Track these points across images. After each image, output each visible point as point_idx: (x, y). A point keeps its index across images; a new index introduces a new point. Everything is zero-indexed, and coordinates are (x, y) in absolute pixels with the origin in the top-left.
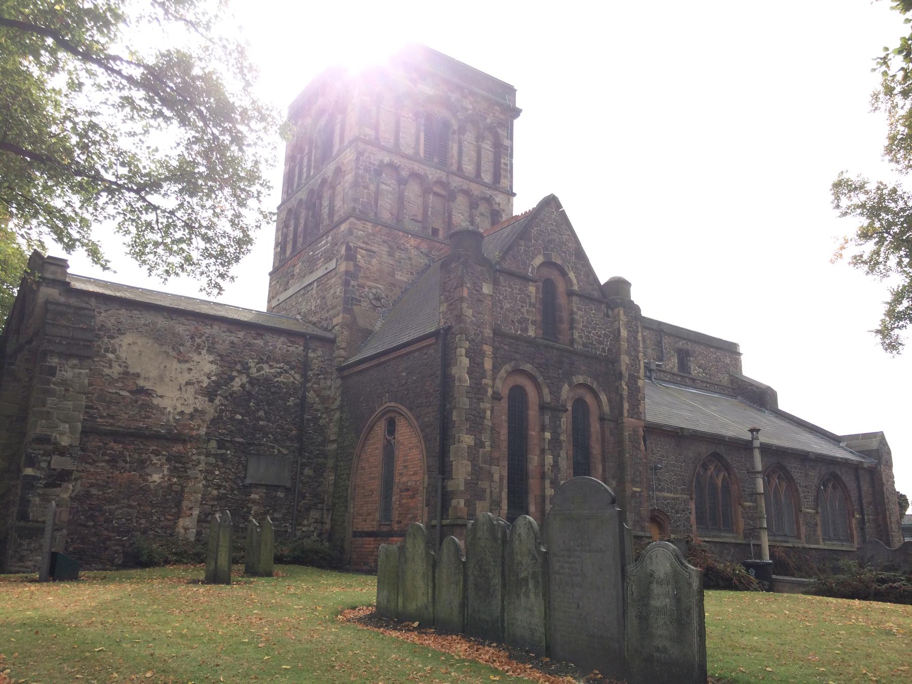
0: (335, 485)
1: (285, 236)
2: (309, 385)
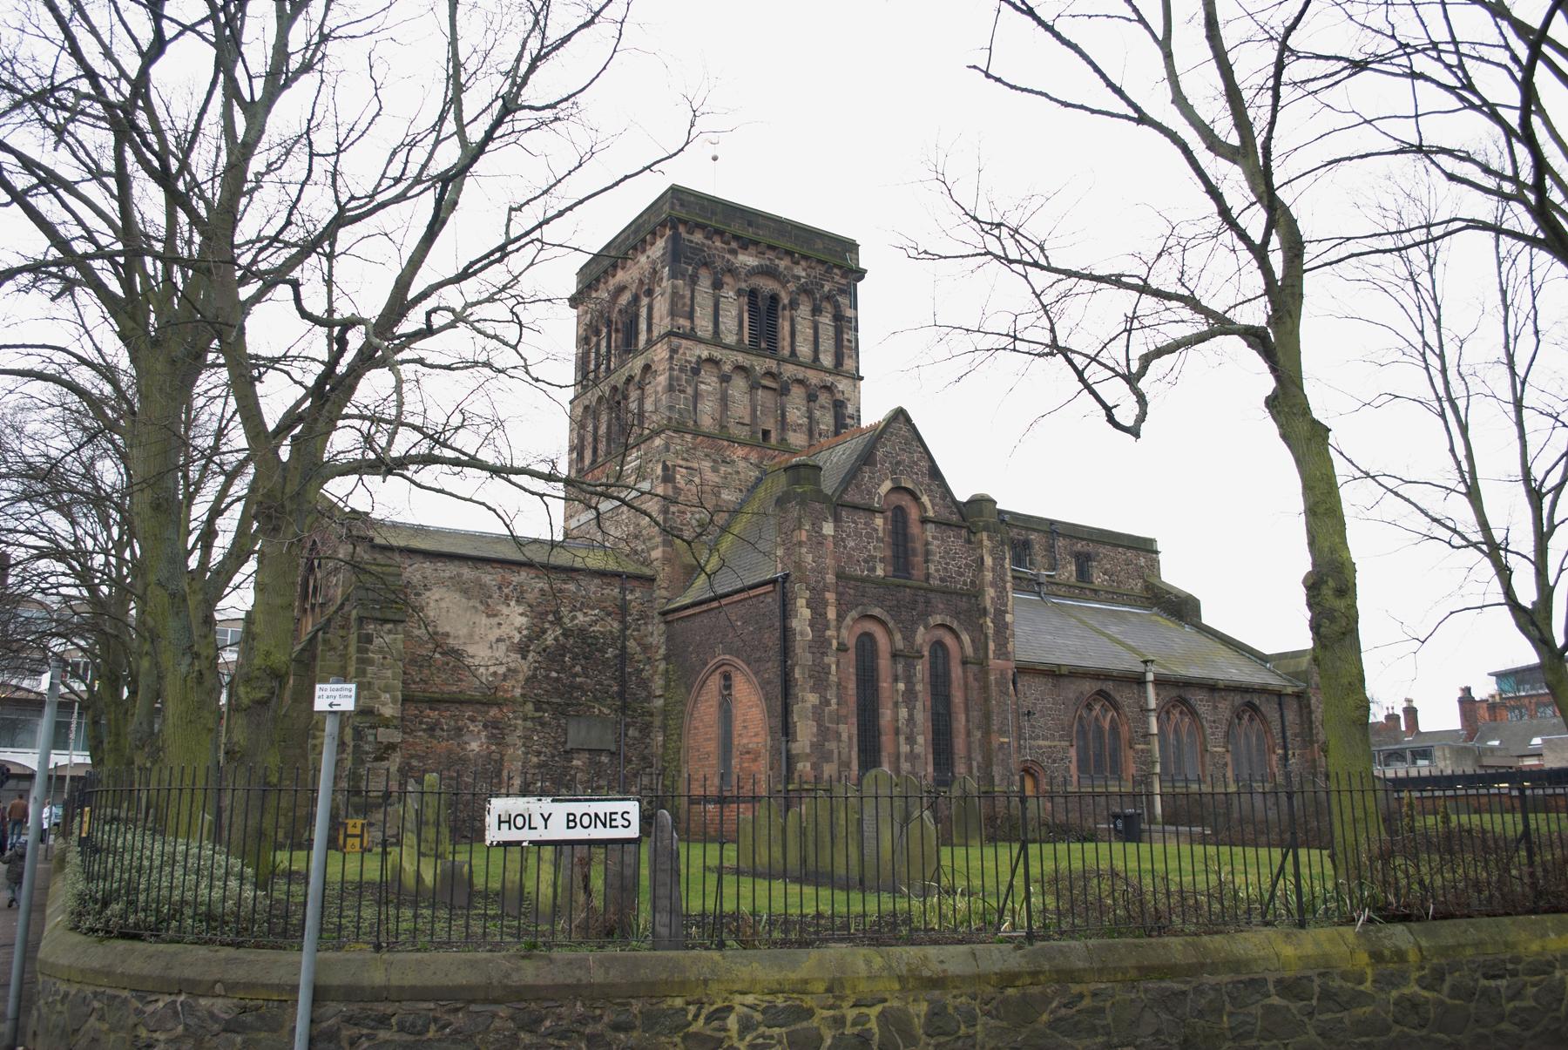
0: (664, 746)
1: (582, 439)
2: (628, 632)
